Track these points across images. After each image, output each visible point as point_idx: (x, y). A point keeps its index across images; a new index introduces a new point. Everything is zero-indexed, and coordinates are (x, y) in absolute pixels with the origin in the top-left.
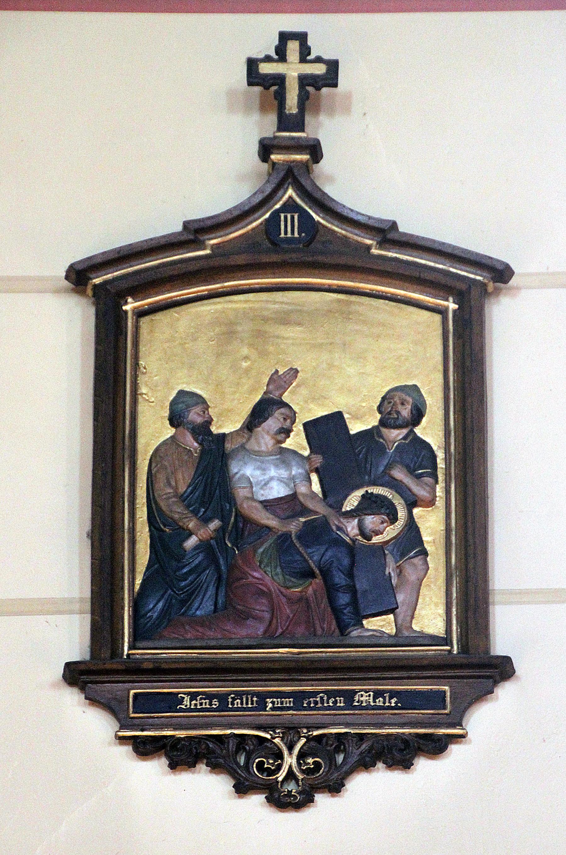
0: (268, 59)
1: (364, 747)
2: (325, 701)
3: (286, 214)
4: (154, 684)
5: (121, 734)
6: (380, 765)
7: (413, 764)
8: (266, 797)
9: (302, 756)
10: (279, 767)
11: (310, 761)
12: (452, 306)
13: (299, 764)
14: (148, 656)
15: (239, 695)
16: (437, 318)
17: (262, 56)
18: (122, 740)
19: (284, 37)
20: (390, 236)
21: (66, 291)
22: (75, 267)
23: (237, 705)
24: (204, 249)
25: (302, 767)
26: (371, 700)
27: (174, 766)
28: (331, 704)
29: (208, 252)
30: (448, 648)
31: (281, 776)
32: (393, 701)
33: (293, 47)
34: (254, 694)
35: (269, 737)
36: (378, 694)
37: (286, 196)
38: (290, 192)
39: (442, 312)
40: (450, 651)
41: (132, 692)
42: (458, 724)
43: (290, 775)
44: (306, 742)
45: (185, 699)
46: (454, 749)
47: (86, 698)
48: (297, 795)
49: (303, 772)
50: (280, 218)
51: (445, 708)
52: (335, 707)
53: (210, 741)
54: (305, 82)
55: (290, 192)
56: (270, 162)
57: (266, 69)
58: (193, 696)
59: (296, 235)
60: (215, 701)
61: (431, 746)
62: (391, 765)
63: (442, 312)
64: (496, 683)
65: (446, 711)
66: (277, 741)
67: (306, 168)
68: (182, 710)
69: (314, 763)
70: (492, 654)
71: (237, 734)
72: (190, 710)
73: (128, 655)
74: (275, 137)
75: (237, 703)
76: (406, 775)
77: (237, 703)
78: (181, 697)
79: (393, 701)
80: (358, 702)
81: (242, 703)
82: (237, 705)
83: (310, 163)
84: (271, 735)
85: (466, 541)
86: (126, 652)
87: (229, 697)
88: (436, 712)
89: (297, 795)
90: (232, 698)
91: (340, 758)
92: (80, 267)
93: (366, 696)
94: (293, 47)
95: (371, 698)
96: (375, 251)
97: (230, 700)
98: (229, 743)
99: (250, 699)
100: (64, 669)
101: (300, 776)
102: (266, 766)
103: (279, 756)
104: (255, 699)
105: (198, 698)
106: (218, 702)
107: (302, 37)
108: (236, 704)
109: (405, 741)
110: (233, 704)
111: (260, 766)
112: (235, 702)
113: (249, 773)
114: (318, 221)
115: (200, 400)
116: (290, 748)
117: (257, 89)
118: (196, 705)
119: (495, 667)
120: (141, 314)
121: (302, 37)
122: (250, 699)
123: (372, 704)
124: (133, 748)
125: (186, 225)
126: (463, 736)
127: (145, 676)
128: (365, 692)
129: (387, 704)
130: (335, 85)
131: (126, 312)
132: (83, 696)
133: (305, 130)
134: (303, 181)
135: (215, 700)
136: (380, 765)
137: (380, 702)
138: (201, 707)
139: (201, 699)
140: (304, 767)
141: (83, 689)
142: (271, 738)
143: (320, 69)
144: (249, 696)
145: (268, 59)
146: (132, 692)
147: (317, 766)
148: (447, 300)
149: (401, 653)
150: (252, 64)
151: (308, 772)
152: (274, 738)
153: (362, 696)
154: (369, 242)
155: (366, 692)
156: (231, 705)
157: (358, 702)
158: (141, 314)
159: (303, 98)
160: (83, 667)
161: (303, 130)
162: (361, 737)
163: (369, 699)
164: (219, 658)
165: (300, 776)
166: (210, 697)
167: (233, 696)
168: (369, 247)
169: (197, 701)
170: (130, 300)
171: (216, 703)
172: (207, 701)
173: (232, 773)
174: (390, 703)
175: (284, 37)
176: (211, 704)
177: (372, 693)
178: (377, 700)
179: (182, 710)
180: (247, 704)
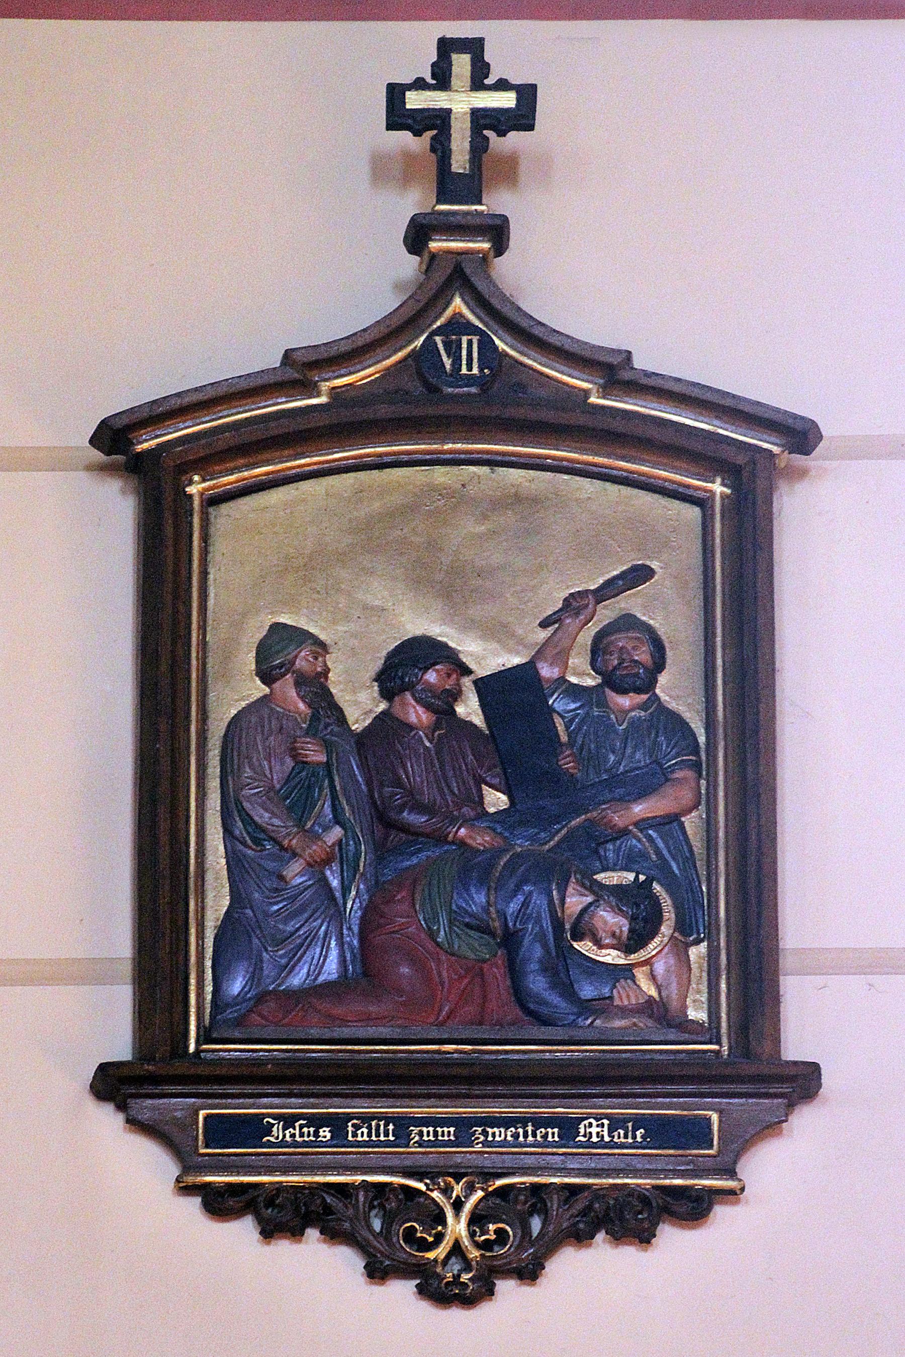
0: (419, 84)
1: (579, 1206)
2: (530, 1133)
3: (470, 337)
4: (187, 1100)
5: (190, 1179)
6: (313, 1234)
7: (655, 1236)
8: (417, 1286)
9: (477, 1220)
10: (439, 1237)
11: (492, 1227)
12: (718, 488)
13: (472, 1235)
14: (516, 1057)
15: (366, 1119)
16: (693, 513)
17: (408, 80)
18: (185, 1189)
19: (446, 47)
20: (626, 375)
21: (90, 468)
22: (111, 423)
23: (362, 1136)
24: (319, 395)
25: (477, 1238)
26: (606, 1133)
27: (268, 1232)
28: (539, 1138)
29: (323, 400)
30: (715, 1047)
31: (440, 1252)
32: (639, 1133)
33: (462, 63)
34: (388, 1119)
35: (421, 1186)
36: (616, 1123)
37: (449, 312)
38: (458, 304)
39: (702, 502)
40: (717, 1053)
41: (202, 1114)
42: (731, 1173)
43: (457, 1249)
44: (484, 1197)
45: (275, 1129)
46: (721, 1212)
47: (128, 1121)
48: (470, 1284)
49: (478, 1245)
50: (436, 343)
51: (711, 1146)
52: (545, 1144)
53: (328, 1193)
54: (482, 122)
55: (458, 304)
56: (426, 256)
57: (415, 100)
58: (289, 1121)
59: (475, 371)
60: (324, 1131)
61: (682, 1208)
62: (618, 1237)
63: (702, 502)
64: (791, 1106)
65: (710, 1152)
66: (435, 1195)
67: (484, 260)
68: (270, 1145)
69: (496, 1232)
70: (784, 1058)
71: (372, 1183)
72: (283, 1144)
73: (198, 1051)
74: (434, 213)
75: (362, 1133)
76: (642, 1254)
77: (362, 1133)
78: (267, 1122)
79: (639, 1133)
80: (585, 1136)
81: (370, 1135)
82: (362, 1136)
83: (492, 254)
84: (426, 1184)
85: (173, 762)
86: (192, 1048)
87: (350, 1124)
88: (680, 1152)
89: (470, 1284)
90: (353, 1125)
91: (536, 1224)
92: (119, 424)
93: (598, 1126)
94: (462, 63)
95: (606, 1129)
96: (593, 400)
97: (350, 1129)
98: (357, 1196)
99: (382, 1128)
100: (95, 1073)
101: (474, 1254)
102: (419, 1235)
103: (440, 1219)
104: (391, 1127)
105: (297, 1124)
106: (330, 1131)
107: (475, 47)
108: (360, 1135)
109: (643, 1198)
110: (355, 1135)
111: (410, 1235)
112: (359, 1132)
113: (390, 1244)
114: (504, 350)
115: (300, 636)
116: (458, 1206)
117: (405, 137)
118: (293, 1136)
119: (791, 1079)
120: (214, 500)
121: (475, 47)
122: (382, 1128)
123: (607, 1139)
124: (202, 1201)
125: (288, 355)
126: (743, 1189)
127: (251, 1087)
128: (594, 1118)
129: (630, 1140)
130: (531, 128)
131: (191, 496)
132: (120, 1118)
133: (484, 201)
134: (481, 285)
135: (324, 1129)
136: (601, 1236)
137: (619, 1136)
138: (386, 1138)
139: (301, 1127)
140: (480, 1236)
141: (121, 1107)
142: (428, 1189)
143: (507, 100)
144: (382, 1123)
145: (419, 84)
146: (202, 1114)
147: (501, 1235)
148: (713, 482)
149: (628, 1055)
150: (395, 93)
151: (486, 1246)
152: (432, 1191)
153: (590, 1125)
154: (585, 385)
155: (597, 1120)
156: (437, 1131)
157: (585, 1136)
158: (214, 500)
159: (479, 147)
160: (125, 1072)
161: (480, 203)
162: (574, 1190)
163: (602, 1131)
164: (419, 1060)
165: (474, 1254)
166: (317, 1122)
167: (355, 1121)
168: (586, 393)
169: (294, 1129)
170: (196, 478)
171: (325, 1133)
172: (312, 1130)
173: (362, 1247)
174: (634, 1137)
175: (446, 47)
176: (316, 1134)
177: (606, 1122)
178: (616, 1133)
179: (270, 1145)
180: (378, 1135)
